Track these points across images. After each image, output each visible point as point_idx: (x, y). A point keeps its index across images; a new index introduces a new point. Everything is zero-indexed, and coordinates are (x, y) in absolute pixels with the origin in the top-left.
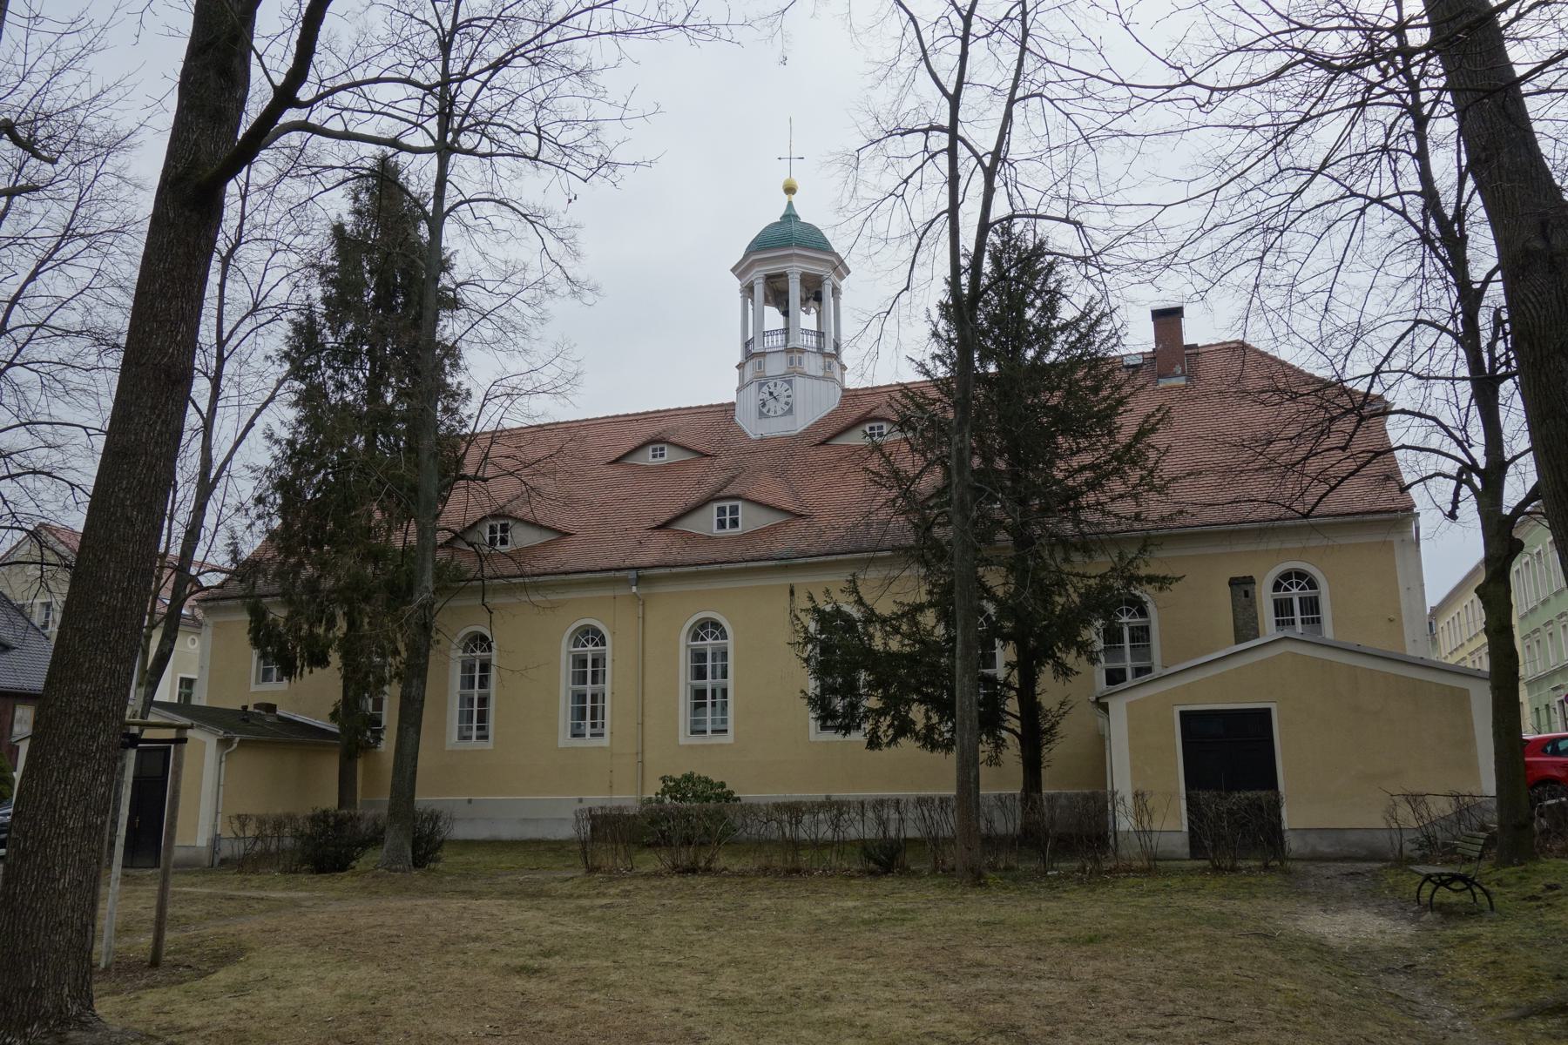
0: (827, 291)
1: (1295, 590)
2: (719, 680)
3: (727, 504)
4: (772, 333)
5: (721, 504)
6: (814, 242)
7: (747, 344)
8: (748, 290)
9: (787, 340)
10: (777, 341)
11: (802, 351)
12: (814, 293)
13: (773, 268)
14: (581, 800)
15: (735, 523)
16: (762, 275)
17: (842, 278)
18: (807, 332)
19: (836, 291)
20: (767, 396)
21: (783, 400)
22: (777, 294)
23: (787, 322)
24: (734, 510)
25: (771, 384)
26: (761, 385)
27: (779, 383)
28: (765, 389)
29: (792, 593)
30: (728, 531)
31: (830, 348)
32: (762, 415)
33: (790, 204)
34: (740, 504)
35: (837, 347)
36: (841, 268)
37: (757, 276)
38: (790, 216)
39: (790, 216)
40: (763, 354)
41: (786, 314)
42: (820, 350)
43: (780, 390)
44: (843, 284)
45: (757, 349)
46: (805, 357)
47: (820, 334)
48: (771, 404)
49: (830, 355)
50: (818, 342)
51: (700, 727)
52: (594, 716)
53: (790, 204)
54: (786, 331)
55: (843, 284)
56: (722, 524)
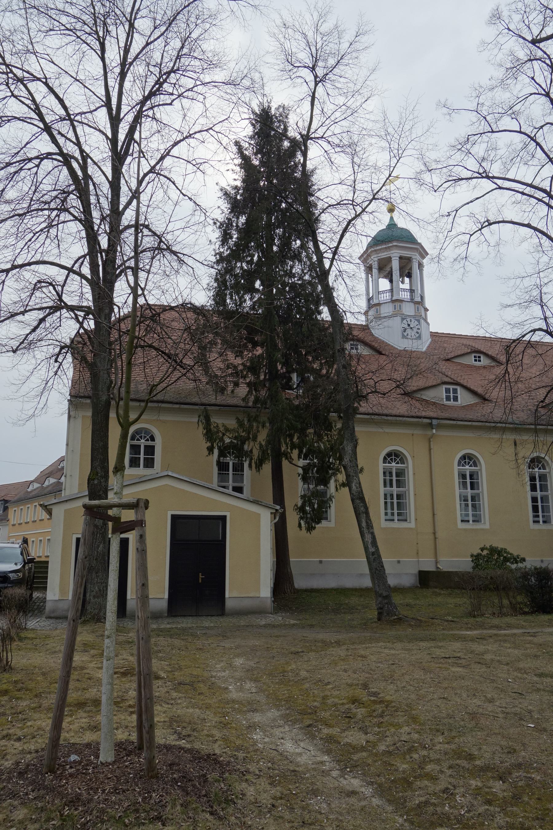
0: (415, 266)
1: (467, 467)
2: (388, 488)
3: (451, 387)
4: (384, 292)
5: (448, 386)
6: (407, 238)
7: (369, 300)
8: (369, 269)
9: (392, 296)
10: (386, 297)
11: (401, 301)
12: (406, 271)
13: (384, 255)
14: (542, 561)
15: (456, 399)
16: (376, 259)
17: (423, 258)
18: (404, 290)
19: (421, 266)
20: (406, 326)
21: (415, 330)
22: (384, 269)
23: (392, 286)
24: (455, 391)
25: (408, 320)
26: (403, 319)
27: (413, 320)
28: (405, 321)
29: (515, 444)
30: (452, 403)
31: (418, 299)
32: (404, 337)
33: (392, 218)
34: (459, 388)
35: (422, 297)
36: (424, 253)
37: (374, 260)
38: (392, 225)
39: (392, 225)
40: (379, 304)
41: (391, 281)
42: (412, 300)
43: (413, 324)
44: (425, 261)
45: (375, 301)
46: (404, 305)
47: (412, 291)
48: (409, 331)
49: (418, 303)
50: (411, 296)
51: (466, 519)
52: (474, 506)
53: (392, 218)
54: (392, 290)
55: (425, 261)
56: (448, 398)
